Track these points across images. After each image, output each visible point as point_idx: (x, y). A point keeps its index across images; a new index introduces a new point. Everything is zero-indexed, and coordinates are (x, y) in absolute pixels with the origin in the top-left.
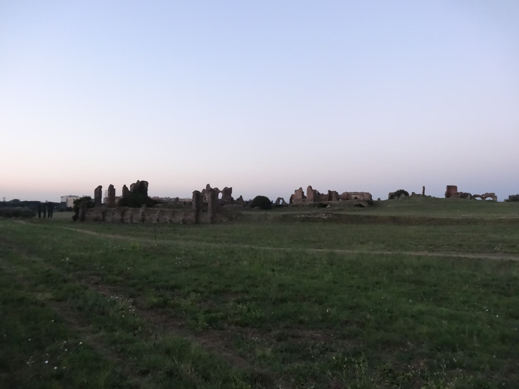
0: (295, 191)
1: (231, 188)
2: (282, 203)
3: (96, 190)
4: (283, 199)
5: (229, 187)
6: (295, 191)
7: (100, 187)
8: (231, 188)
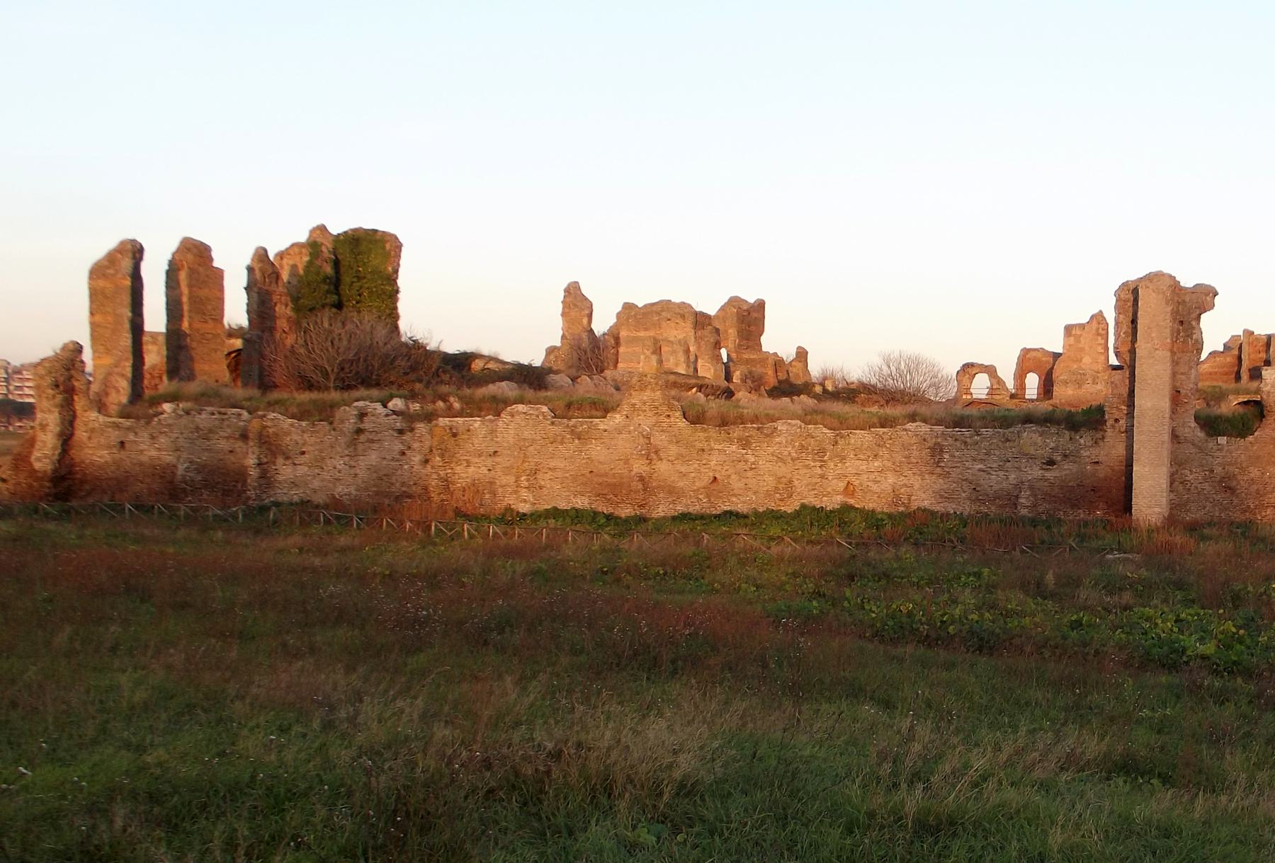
0: (1069, 329)
1: (761, 305)
2: (992, 391)
3: (98, 272)
4: (991, 371)
5: (751, 299)
6: (1069, 329)
7: (136, 252)
8: (761, 305)
